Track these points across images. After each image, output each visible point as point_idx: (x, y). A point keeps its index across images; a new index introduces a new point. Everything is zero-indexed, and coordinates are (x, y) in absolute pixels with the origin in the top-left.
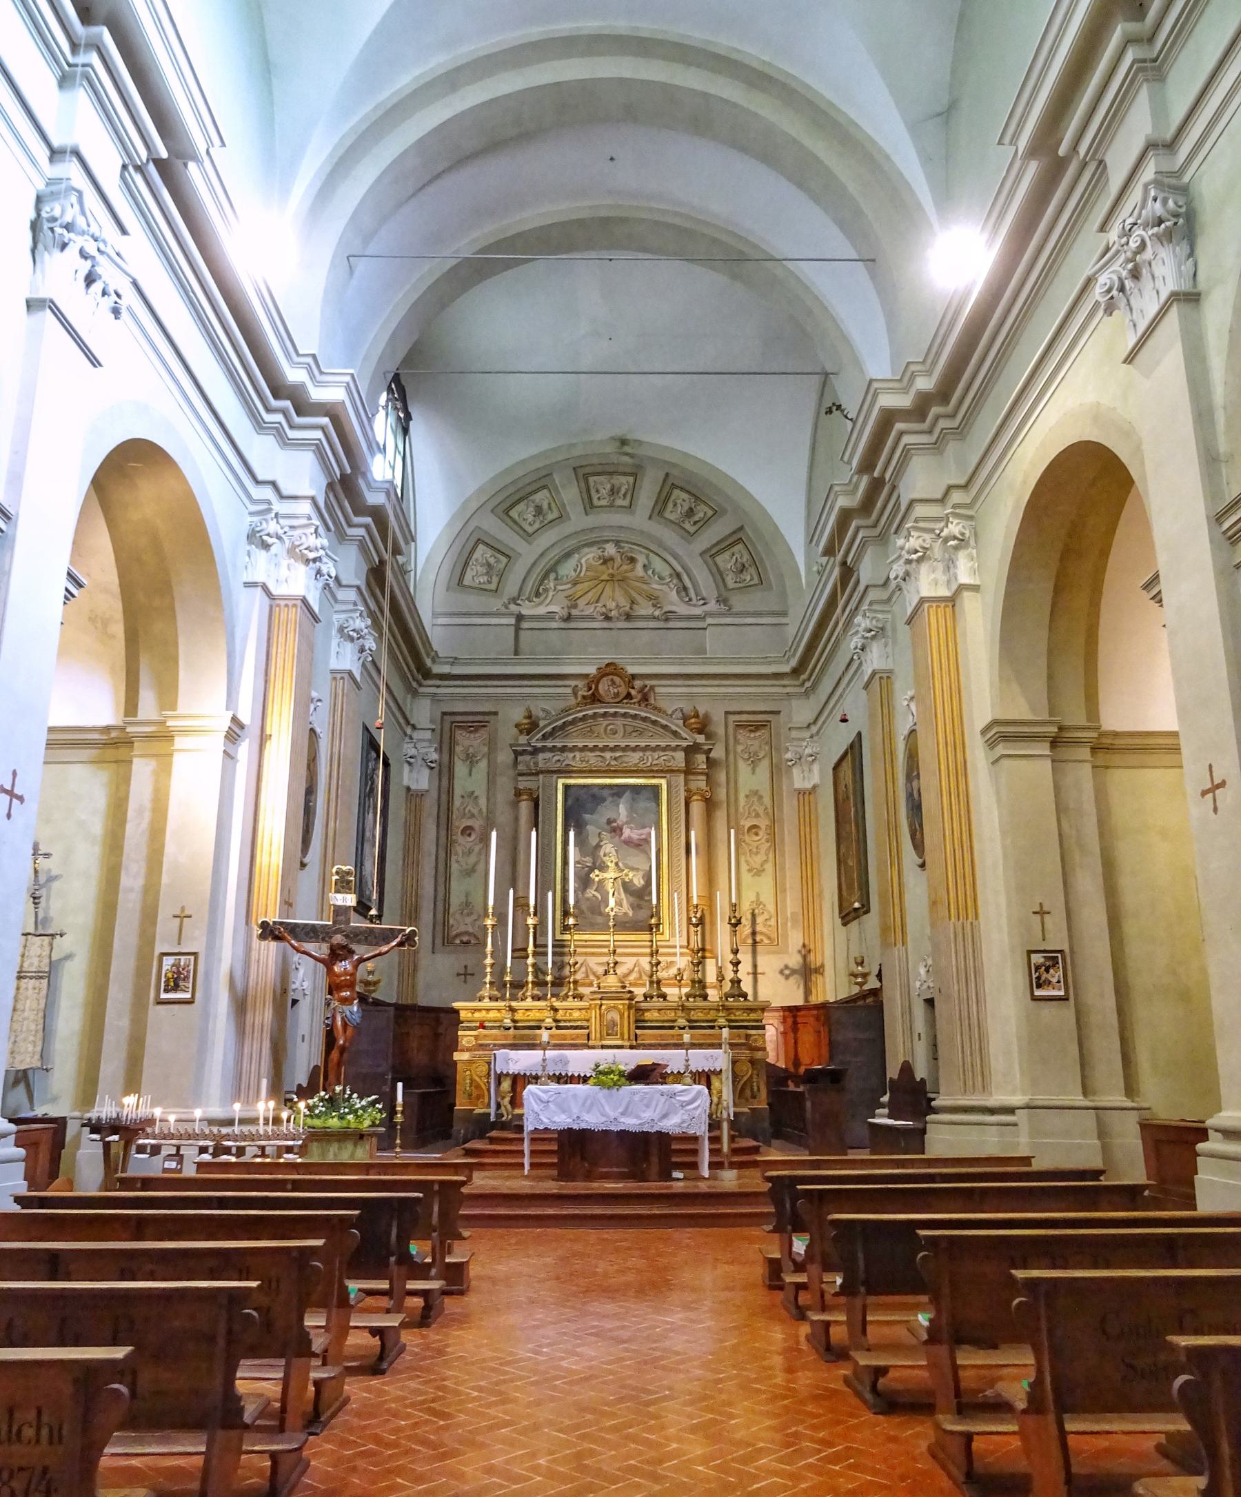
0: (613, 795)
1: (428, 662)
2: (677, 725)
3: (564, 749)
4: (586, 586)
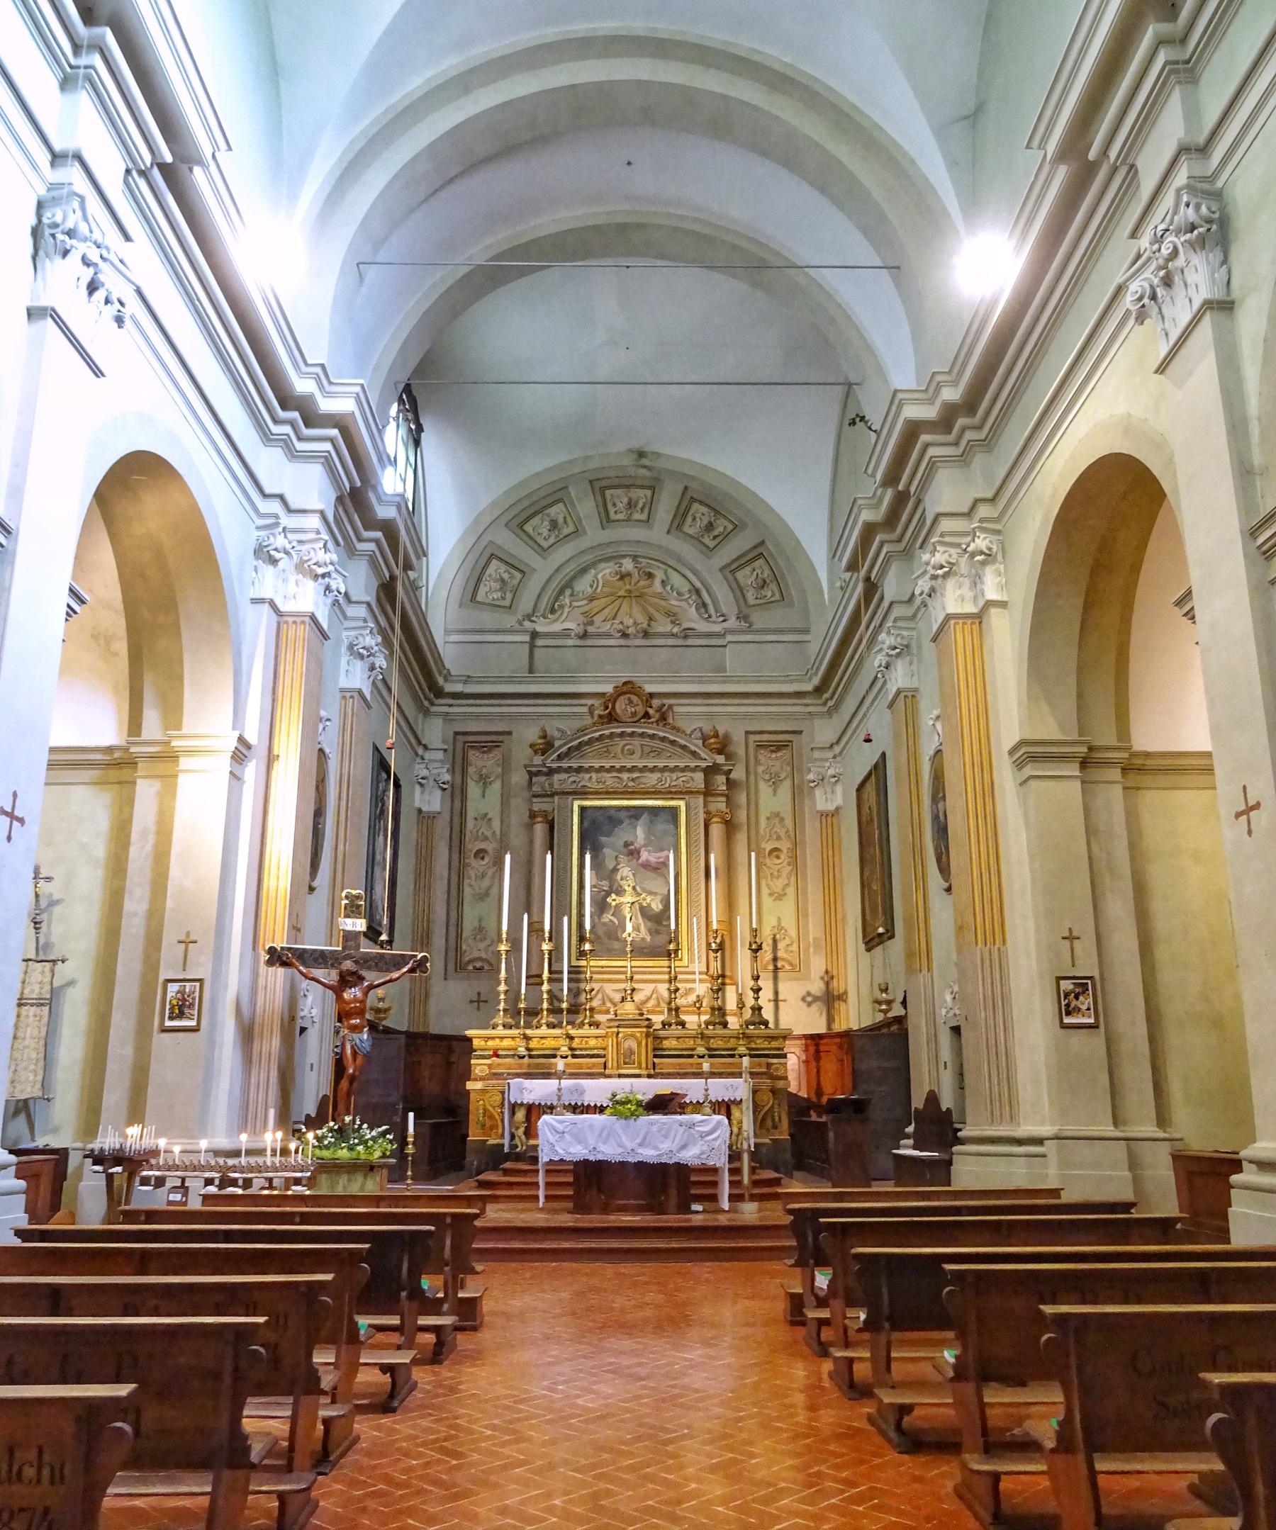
0: (630, 817)
1: (440, 681)
3: (579, 770)
4: (602, 602)
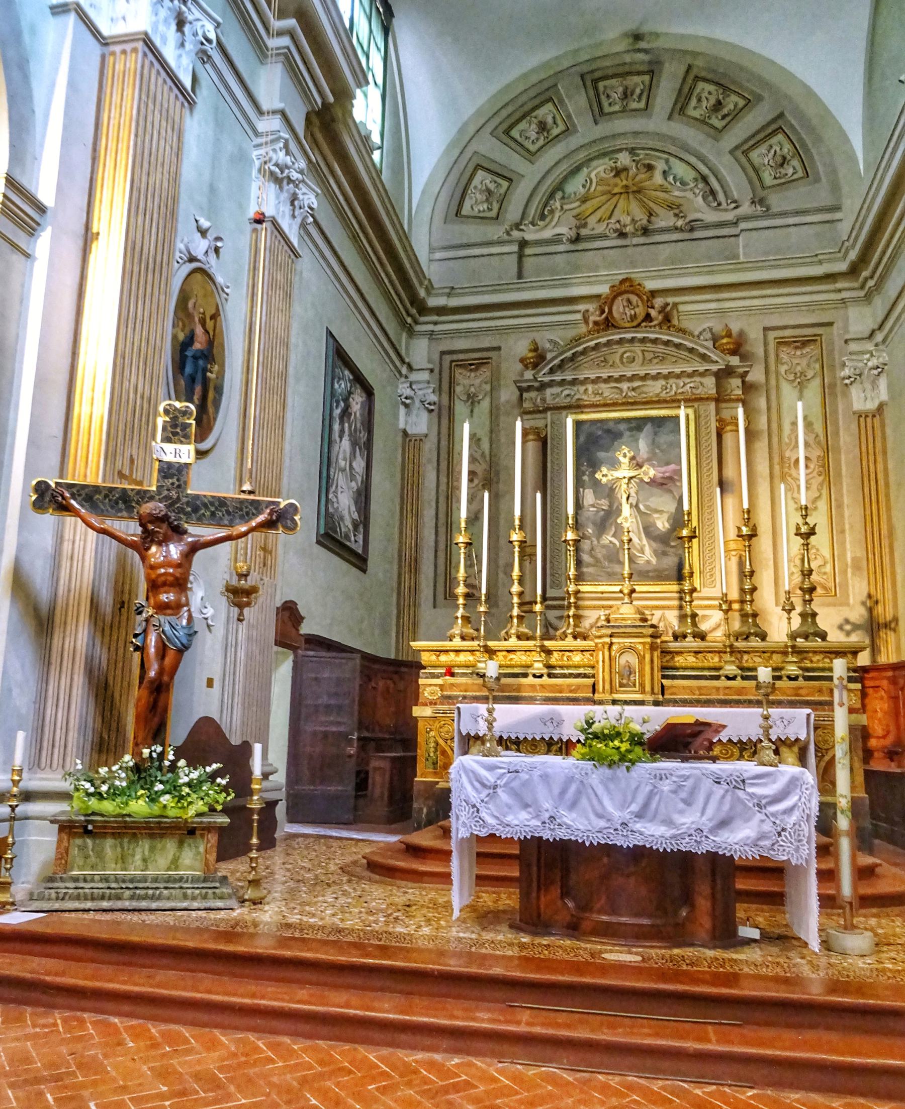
0: (630, 429)
1: (422, 293)
2: (707, 348)
3: (574, 382)
4: (595, 202)
